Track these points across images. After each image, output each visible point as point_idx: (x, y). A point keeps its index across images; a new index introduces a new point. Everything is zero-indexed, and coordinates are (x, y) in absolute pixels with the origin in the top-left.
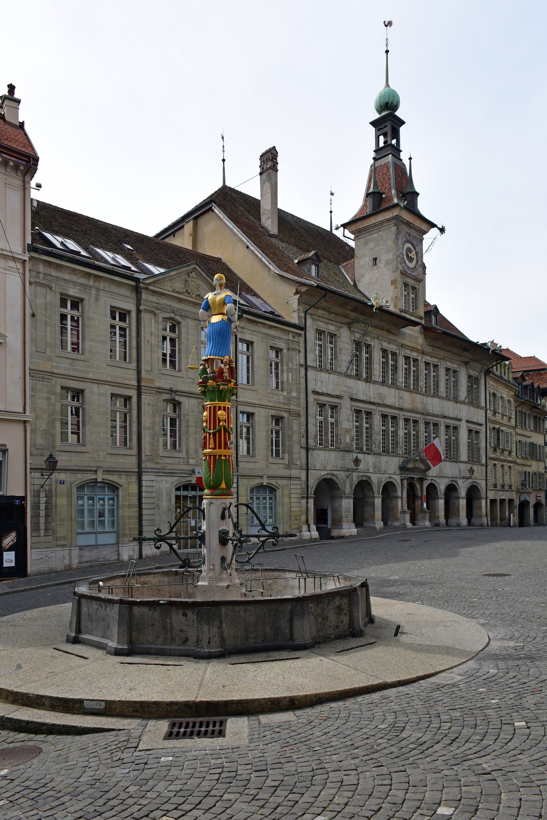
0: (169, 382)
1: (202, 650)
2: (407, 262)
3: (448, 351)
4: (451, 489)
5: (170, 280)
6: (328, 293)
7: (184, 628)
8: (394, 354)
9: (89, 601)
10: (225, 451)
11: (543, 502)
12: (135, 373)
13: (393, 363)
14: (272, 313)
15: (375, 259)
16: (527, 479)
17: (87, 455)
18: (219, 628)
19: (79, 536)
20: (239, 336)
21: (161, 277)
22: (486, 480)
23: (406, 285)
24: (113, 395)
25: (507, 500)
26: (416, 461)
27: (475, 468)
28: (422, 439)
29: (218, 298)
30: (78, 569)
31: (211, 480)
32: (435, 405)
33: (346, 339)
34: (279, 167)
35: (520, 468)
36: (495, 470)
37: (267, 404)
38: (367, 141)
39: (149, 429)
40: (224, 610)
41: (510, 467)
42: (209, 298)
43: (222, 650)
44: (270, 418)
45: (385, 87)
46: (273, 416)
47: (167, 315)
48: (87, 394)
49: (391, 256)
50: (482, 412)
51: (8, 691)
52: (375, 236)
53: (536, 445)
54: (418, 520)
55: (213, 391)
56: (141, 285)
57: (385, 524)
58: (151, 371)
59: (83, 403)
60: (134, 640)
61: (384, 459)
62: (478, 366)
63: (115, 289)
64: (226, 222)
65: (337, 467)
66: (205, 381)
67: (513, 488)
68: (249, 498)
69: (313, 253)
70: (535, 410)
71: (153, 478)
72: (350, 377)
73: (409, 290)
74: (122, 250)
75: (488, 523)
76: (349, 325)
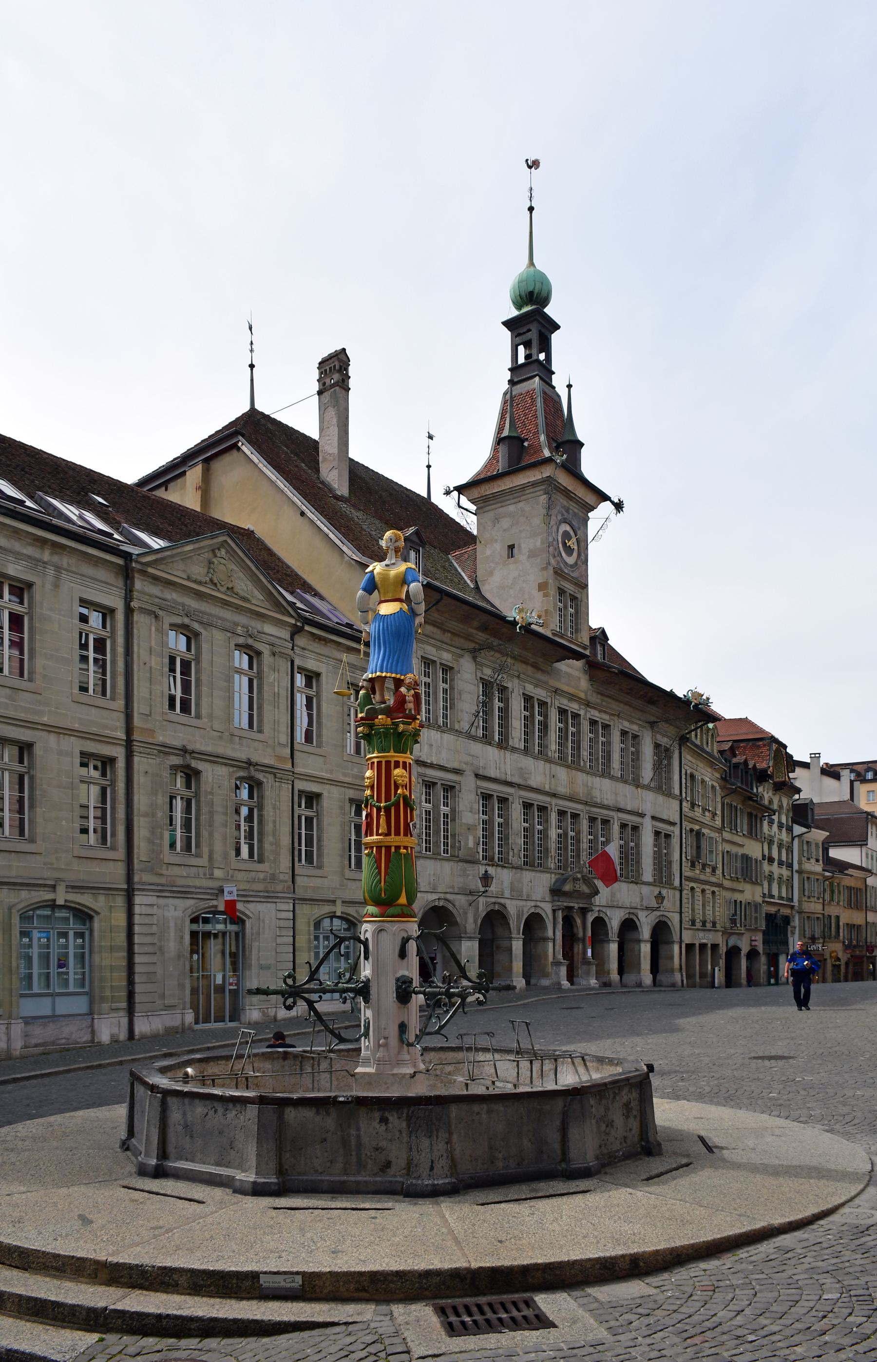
0: (181, 735)
1: (420, 1182)
2: (563, 554)
3: (626, 704)
4: (629, 926)
5: (182, 560)
6: (445, 597)
7: (383, 1144)
8: (543, 704)
9: (187, 1101)
10: (406, 839)
11: (760, 949)
12: (122, 717)
13: (541, 718)
14: (349, 626)
15: (511, 547)
16: (738, 912)
17: (38, 857)
18: (447, 1143)
19: (23, 1001)
20: (297, 662)
21: (169, 553)
22: (681, 913)
23: (561, 592)
24: (83, 754)
25: (709, 945)
26: (576, 879)
27: (664, 892)
28: (584, 845)
29: (393, 572)
30: (22, 1057)
31: (381, 890)
32: (605, 790)
33: (468, 676)
34: (352, 383)
35: (728, 895)
36: (693, 896)
37: (342, 778)
38: (498, 352)
39: (146, 815)
40: (454, 1110)
41: (713, 892)
42: (375, 572)
43: (454, 1180)
44: (348, 805)
45: (528, 267)
46: (351, 801)
47: (178, 620)
48: (38, 750)
49: (539, 544)
50: (675, 804)
51: (97, 1262)
52: (512, 508)
53: (751, 858)
54: (578, 976)
55: (386, 735)
56: (134, 565)
57: (528, 983)
58: (150, 715)
59: (31, 766)
60: (286, 1167)
61: (527, 876)
62: (671, 730)
63: (88, 570)
64: (264, 469)
65: (453, 887)
66: (371, 715)
67: (718, 926)
68: (312, 937)
69: (412, 530)
70: (751, 803)
71: (153, 900)
72: (474, 738)
73: (566, 600)
74: (90, 505)
75: (682, 981)
76: (474, 653)
